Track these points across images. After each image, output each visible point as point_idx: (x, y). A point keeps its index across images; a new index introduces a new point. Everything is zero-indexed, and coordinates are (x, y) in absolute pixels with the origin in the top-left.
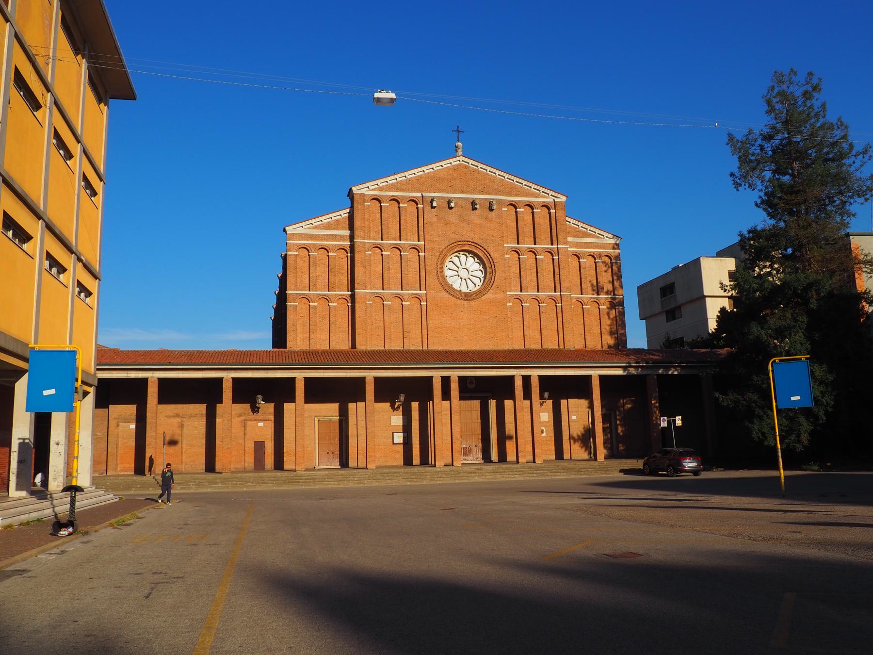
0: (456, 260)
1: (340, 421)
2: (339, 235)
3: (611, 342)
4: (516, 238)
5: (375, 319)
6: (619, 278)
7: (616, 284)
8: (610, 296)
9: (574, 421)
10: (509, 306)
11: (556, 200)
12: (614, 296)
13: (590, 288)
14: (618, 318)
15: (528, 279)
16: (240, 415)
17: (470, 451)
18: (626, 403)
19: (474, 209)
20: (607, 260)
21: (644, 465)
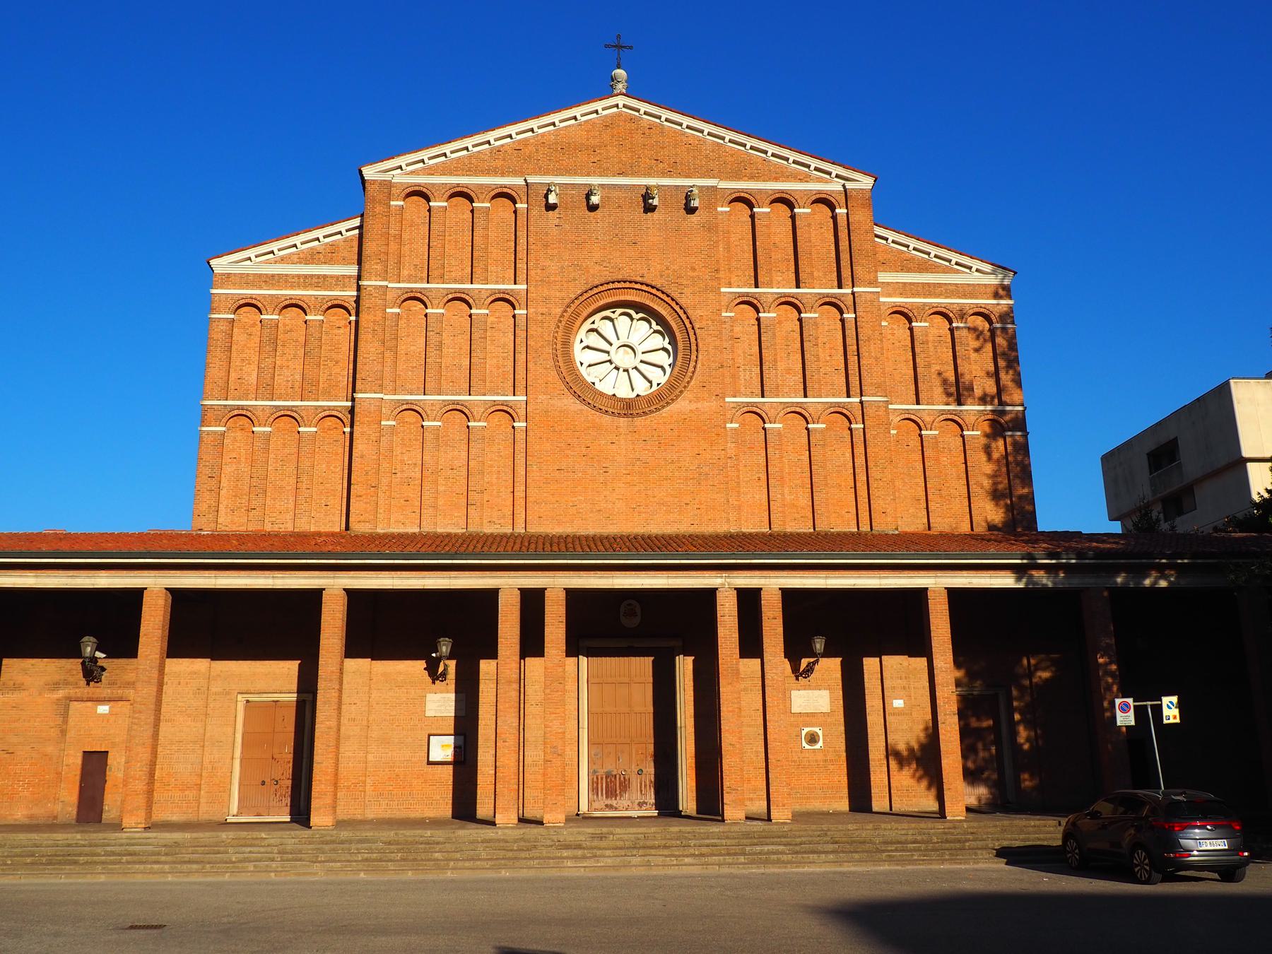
0: (606, 328)
1: (300, 705)
2: (332, 277)
3: (995, 514)
4: (753, 274)
5: (402, 461)
6: (1013, 363)
7: (1006, 378)
8: (989, 408)
9: (899, 712)
10: (732, 429)
11: (849, 185)
12: (1000, 408)
13: (938, 391)
14: (1010, 459)
15: (781, 366)
16: (56, 686)
17: (625, 785)
18: (1037, 668)
19: (649, 209)
20: (980, 322)
21: (1067, 836)
